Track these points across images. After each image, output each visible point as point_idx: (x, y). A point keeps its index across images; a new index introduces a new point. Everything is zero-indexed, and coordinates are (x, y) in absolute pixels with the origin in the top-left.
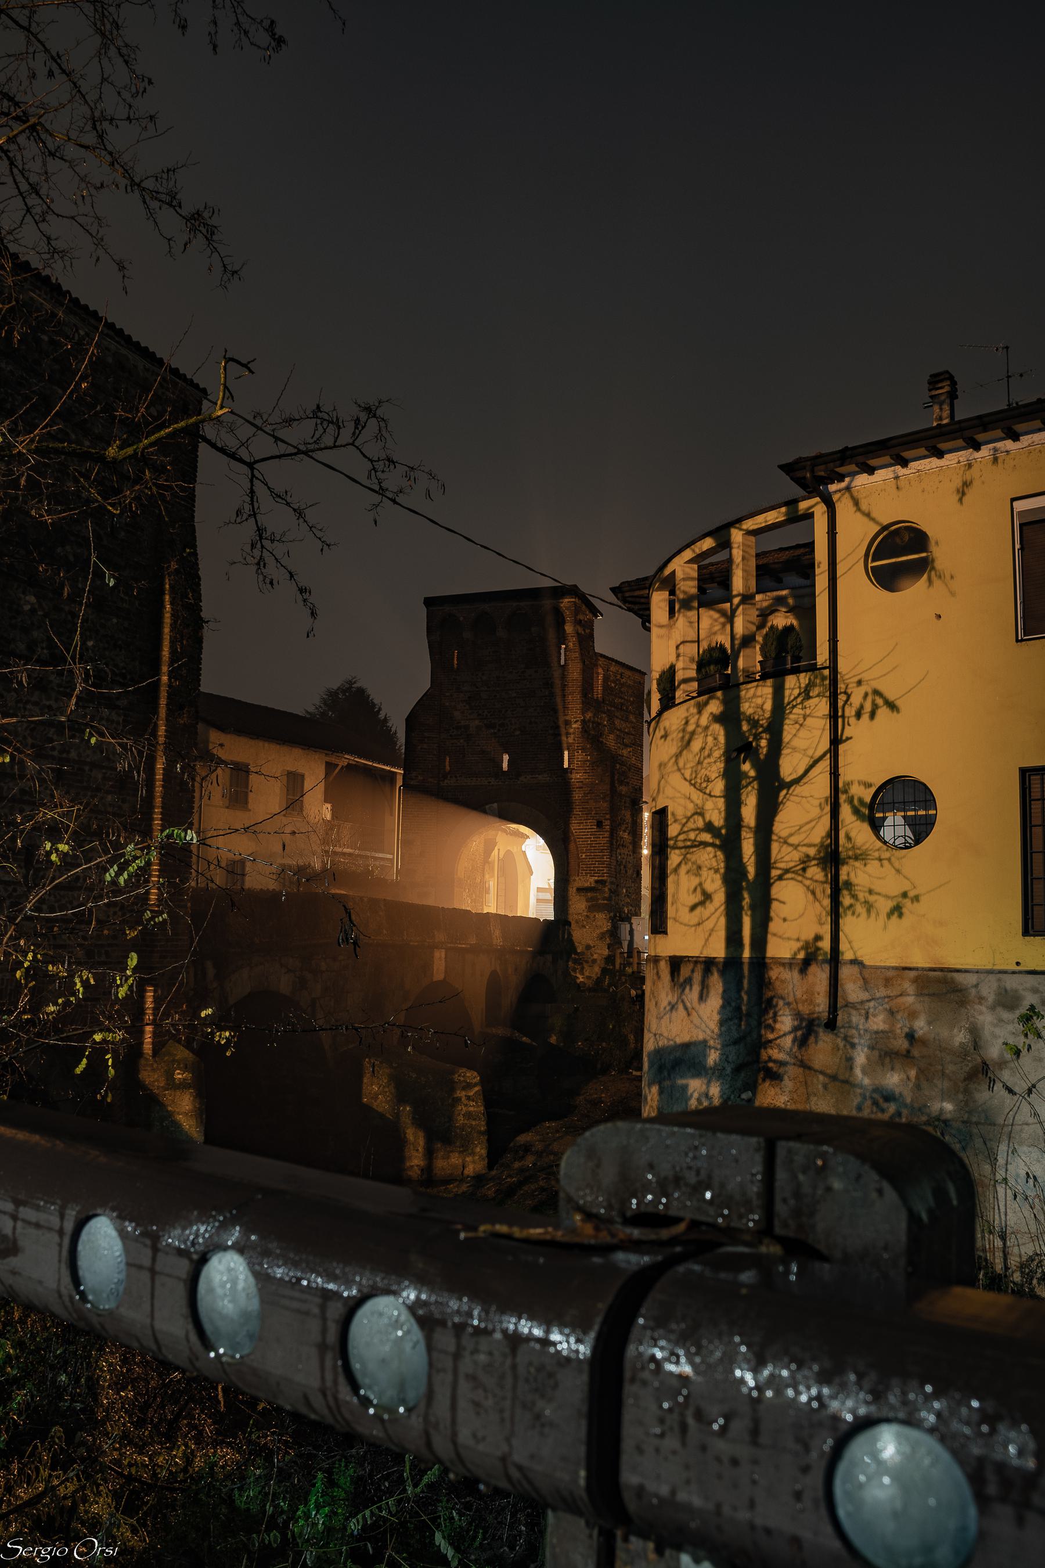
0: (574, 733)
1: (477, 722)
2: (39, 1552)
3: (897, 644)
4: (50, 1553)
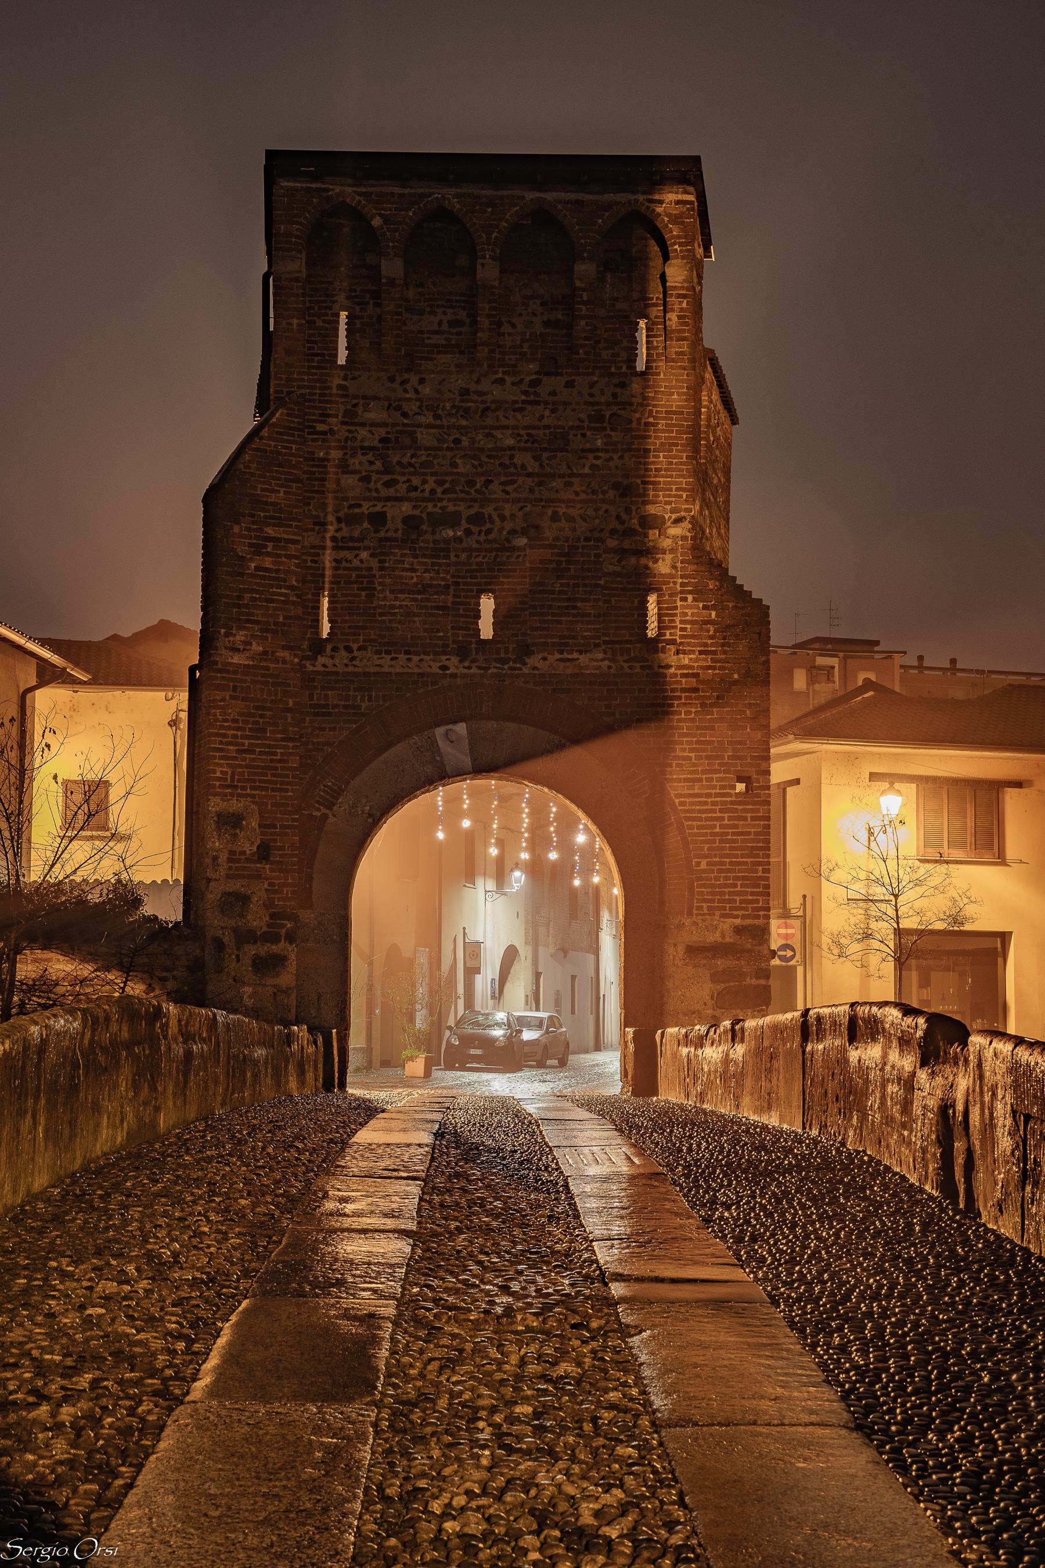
0: (672, 550)
1: (406, 508)
3: (573, 978)
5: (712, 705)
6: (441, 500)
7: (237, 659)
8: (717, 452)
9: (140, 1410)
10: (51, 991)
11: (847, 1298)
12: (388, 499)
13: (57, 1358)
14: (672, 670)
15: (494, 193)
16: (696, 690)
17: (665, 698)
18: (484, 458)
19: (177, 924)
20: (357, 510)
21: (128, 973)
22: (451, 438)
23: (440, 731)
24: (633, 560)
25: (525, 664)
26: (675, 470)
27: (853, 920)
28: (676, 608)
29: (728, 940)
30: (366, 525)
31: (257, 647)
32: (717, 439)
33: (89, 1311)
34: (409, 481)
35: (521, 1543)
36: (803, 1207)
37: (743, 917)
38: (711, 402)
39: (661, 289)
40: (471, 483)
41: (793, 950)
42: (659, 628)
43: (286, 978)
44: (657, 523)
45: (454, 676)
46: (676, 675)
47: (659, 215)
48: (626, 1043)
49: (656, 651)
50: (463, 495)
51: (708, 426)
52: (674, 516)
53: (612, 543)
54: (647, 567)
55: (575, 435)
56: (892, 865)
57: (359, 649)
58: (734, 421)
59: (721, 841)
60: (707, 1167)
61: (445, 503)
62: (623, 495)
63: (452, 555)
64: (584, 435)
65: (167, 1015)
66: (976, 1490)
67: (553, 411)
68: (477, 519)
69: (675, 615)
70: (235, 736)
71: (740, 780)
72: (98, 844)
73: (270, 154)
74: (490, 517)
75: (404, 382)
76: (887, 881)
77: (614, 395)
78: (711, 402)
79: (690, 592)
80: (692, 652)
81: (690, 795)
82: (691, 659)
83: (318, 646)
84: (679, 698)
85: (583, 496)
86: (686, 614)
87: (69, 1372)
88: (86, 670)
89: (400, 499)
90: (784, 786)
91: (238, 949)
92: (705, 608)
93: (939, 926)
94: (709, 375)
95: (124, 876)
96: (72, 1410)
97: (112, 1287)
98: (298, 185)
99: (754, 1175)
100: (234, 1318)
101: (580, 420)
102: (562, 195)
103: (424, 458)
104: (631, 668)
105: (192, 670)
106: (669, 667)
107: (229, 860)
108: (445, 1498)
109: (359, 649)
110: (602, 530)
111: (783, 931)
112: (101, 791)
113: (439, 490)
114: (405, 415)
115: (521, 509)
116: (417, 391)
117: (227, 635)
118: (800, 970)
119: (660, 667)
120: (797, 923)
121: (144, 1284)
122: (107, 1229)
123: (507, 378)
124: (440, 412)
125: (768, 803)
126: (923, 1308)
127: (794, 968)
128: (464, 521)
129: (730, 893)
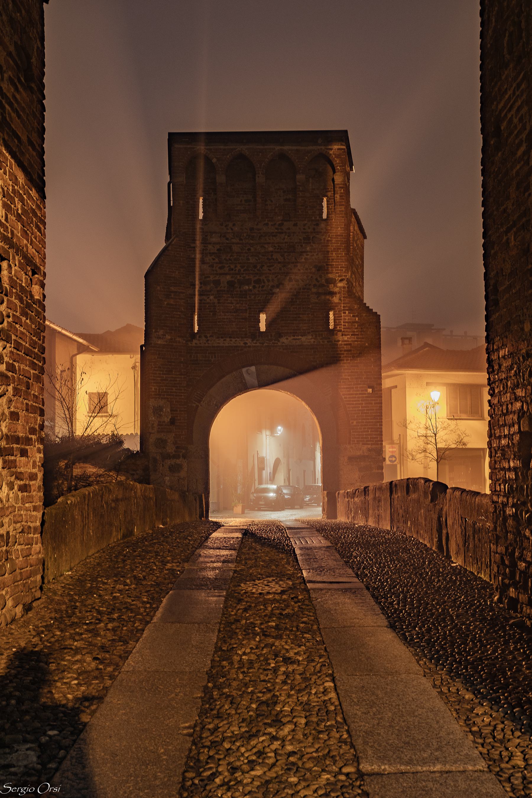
0: (339, 293)
1: (228, 278)
2: (20, 790)
3: (304, 471)
4: (25, 791)
5: (357, 357)
6: (243, 274)
7: (160, 342)
8: (358, 251)
9: (135, 625)
10: (87, 480)
11: (395, 587)
12: (221, 274)
13: (105, 609)
14: (340, 342)
15: (262, 147)
16: (350, 351)
17: (338, 354)
18: (260, 256)
19: (138, 452)
20: (208, 279)
21: (118, 472)
22: (247, 248)
23: (244, 370)
24: (323, 297)
25: (279, 341)
26: (340, 259)
27: (418, 445)
28: (341, 317)
29: (365, 454)
30: (212, 285)
31: (168, 337)
32: (357, 245)
33: (114, 595)
34: (229, 266)
35: (269, 662)
36: (385, 557)
37: (372, 444)
38: (354, 230)
39: (332, 185)
40: (255, 267)
41: (396, 458)
42: (335, 325)
43: (183, 474)
44: (333, 282)
45: (249, 347)
46: (342, 344)
47: (331, 154)
48: (324, 497)
49: (333, 334)
50: (252, 272)
51: (353, 240)
52: (340, 279)
53: (314, 290)
54: (329, 300)
55: (298, 246)
56: (433, 421)
57: (210, 337)
58: (365, 237)
59: (362, 413)
60: (350, 544)
61: (244, 275)
62: (318, 270)
63: (248, 297)
64: (302, 246)
65: (136, 488)
66: (428, 644)
67: (288, 236)
68: (258, 281)
69: (341, 319)
70: (160, 374)
71: (369, 387)
72: (105, 419)
73: (170, 134)
74: (263, 280)
75: (226, 226)
76: (431, 428)
77: (314, 229)
78: (354, 230)
79: (347, 310)
80: (349, 335)
81: (349, 394)
82: (348, 338)
83: (193, 335)
84: (343, 354)
85: (302, 271)
86: (346, 319)
87: (110, 613)
88: (97, 346)
89: (226, 274)
90: (390, 389)
91: (163, 461)
92: (353, 316)
93: (453, 446)
94: (353, 219)
95: (115, 433)
96: (112, 625)
97: (122, 587)
98: (182, 146)
99: (368, 546)
100: (167, 596)
101: (300, 240)
102: (291, 147)
103: (235, 257)
104: (323, 342)
105: (142, 347)
106: (339, 341)
107: (158, 425)
108: (243, 650)
109: (210, 337)
110: (310, 285)
111: (391, 450)
112: (105, 398)
113: (242, 270)
114: (227, 239)
115: (276, 277)
116: (232, 229)
117: (156, 332)
118: (398, 466)
119: (335, 341)
120: (397, 446)
121: (133, 586)
122: (118, 568)
123: (269, 223)
124: (242, 237)
125: (381, 397)
126: (423, 589)
127: (396, 465)
128: (252, 282)
129: (366, 435)
